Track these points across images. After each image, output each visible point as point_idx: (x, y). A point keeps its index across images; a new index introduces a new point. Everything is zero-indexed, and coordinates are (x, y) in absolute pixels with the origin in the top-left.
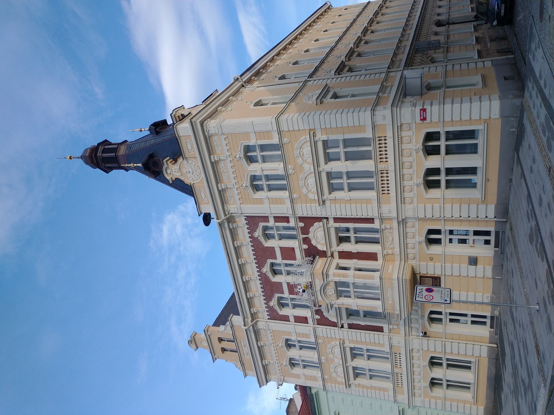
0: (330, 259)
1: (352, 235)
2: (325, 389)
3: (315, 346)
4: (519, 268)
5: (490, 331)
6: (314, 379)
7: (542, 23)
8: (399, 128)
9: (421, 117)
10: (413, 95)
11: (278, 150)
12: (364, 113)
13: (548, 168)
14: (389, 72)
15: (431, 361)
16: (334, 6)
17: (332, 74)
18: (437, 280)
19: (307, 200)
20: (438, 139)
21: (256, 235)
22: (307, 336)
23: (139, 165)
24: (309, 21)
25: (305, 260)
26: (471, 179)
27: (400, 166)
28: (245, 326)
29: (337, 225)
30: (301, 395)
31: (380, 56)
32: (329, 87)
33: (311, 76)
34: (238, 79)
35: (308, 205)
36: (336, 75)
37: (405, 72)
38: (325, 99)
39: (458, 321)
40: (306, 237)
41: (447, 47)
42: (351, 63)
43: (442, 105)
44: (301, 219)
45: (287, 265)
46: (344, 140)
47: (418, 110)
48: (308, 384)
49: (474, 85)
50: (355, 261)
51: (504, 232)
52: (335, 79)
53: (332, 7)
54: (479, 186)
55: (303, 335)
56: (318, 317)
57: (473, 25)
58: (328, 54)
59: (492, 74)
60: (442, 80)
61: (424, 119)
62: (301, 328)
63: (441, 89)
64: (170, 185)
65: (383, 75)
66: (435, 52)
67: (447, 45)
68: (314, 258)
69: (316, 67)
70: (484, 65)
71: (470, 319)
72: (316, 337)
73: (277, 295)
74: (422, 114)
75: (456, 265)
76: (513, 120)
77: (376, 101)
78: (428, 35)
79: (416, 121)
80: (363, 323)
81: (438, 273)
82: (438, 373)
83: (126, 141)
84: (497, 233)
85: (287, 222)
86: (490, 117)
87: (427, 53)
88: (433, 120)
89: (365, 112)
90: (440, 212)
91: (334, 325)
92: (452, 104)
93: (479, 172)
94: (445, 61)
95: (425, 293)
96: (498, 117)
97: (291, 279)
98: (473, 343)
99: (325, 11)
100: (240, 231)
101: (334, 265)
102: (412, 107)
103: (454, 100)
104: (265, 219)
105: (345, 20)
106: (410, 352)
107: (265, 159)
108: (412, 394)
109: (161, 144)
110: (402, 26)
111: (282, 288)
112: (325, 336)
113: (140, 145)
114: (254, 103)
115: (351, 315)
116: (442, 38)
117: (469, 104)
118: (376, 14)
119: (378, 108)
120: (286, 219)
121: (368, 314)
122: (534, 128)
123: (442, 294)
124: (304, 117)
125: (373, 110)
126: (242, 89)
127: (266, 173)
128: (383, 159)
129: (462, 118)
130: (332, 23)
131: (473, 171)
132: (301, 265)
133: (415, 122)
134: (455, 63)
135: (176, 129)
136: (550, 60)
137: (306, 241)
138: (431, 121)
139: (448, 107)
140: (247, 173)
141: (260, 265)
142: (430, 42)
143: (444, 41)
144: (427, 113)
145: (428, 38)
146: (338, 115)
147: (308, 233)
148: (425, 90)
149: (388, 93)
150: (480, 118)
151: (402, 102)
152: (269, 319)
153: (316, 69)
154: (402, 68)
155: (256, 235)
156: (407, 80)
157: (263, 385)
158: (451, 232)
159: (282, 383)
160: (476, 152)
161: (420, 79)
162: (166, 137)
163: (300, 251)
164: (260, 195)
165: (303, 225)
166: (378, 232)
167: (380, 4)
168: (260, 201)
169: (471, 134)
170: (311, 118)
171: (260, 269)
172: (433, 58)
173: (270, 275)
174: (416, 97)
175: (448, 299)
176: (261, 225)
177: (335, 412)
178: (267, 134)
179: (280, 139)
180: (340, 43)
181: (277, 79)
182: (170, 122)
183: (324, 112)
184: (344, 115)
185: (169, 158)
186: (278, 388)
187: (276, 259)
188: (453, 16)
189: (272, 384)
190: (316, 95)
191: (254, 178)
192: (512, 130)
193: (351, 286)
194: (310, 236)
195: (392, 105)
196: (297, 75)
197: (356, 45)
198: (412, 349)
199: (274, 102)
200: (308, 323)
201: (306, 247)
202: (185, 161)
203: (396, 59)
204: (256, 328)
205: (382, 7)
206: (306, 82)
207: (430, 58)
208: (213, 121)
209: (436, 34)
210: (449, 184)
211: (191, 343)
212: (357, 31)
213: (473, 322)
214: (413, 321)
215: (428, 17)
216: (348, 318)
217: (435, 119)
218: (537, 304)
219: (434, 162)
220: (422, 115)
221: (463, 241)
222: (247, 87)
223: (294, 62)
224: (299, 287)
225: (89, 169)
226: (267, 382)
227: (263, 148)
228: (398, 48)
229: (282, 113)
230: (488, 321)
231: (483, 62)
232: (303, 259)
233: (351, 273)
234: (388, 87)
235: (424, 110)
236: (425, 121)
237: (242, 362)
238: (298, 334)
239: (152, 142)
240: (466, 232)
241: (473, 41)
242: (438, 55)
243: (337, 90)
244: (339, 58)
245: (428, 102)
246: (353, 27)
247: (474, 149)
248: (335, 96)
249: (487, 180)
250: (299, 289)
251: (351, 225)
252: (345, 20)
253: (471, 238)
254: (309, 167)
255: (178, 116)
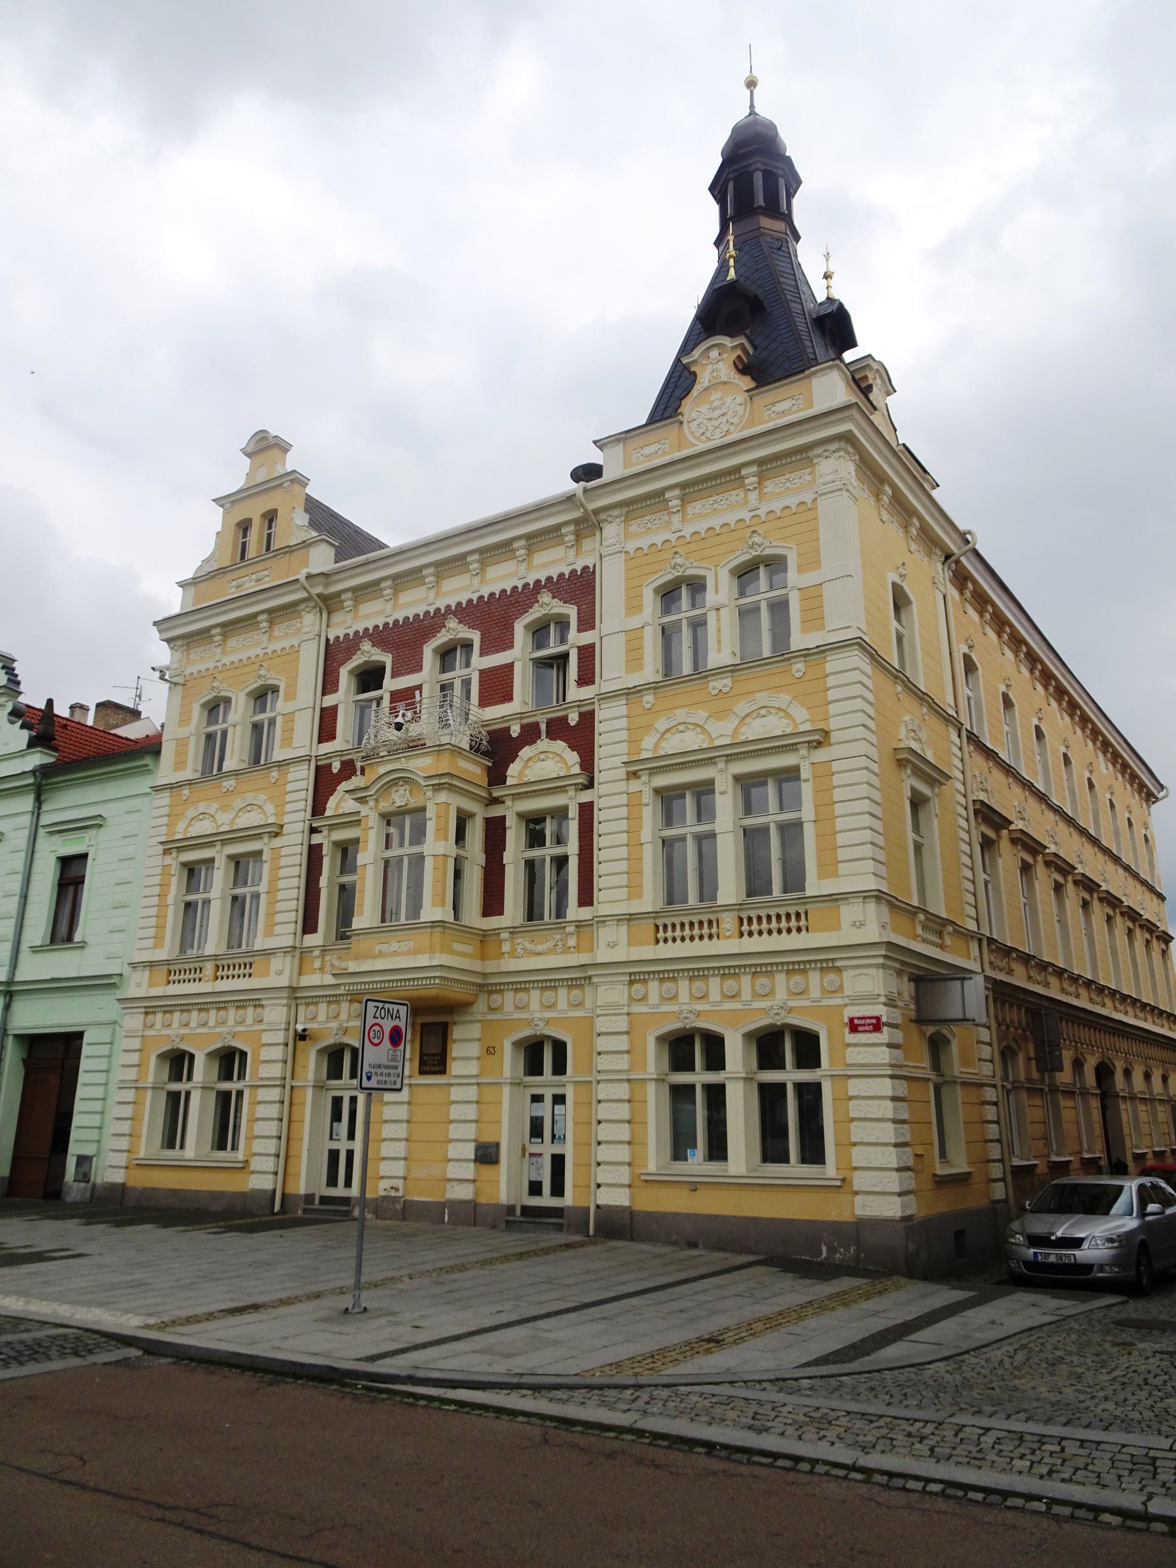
0: (484, 794)
1: (549, 851)
2: (157, 789)
3: (262, 762)
4: (463, 1265)
5: (314, 1194)
6: (180, 765)
7: (1112, 1325)
8: (830, 965)
9: (859, 1018)
10: (918, 999)
11: (774, 648)
12: (872, 871)
13: (720, 1338)
14: (980, 940)
15: (235, 1053)
16: (1154, 808)
17: (977, 793)
18: (439, 1065)
19: (635, 735)
20: (800, 1064)
21: (545, 597)
22: (287, 741)
23: (732, 274)
24: (1118, 743)
25: (481, 729)
26: (694, 1146)
27: (728, 968)
28: (309, 577)
29: (573, 812)
30: (147, 736)
31: (1021, 921)
32: (941, 784)
33: (973, 739)
34: (968, 542)
35: (624, 735)
36: (974, 805)
37: (980, 979)
38: (909, 771)
39: (336, 1116)
40: (540, 732)
41: (1041, 1090)
42: (1005, 844)
43: (890, 1072)
44: (588, 719)
45: (467, 683)
46: (798, 825)
47: (880, 1010)
48: (167, 749)
49: (943, 1154)
50: (481, 859)
51: (559, 1228)
52: (962, 800)
53: (1154, 803)
54: (679, 1166)
55: (289, 731)
56: (336, 767)
57: (1100, 1158)
58: (1029, 787)
59: (972, 1200)
60: (956, 1073)
61: (854, 1027)
62: (306, 726)
63: (934, 1071)
64: (678, 360)
65: (972, 926)
66: (1030, 1059)
67: (1047, 1090)
68: (485, 754)
69: (997, 754)
70: (996, 1180)
71: (343, 1146)
72: (283, 764)
73: (387, 659)
74: (868, 1021)
75: (471, 1112)
76: (849, 1252)
77: (902, 905)
78: (1076, 1042)
79: (849, 1008)
80: (323, 881)
81: (455, 1068)
82: (203, 1072)
83: (797, 238)
84: (558, 1212)
85: (579, 679)
86: (857, 1193)
87: (1027, 1040)
88: (850, 1049)
89: (874, 874)
90: (610, 1071)
91: (318, 808)
92: (894, 1099)
93: (714, 1167)
94: (1006, 1084)
95: (388, 1025)
96: (859, 1212)
97: (428, 698)
98: (282, 1154)
99: (1142, 786)
100: (557, 553)
101: (469, 805)
102: (886, 996)
103: (904, 1104)
104: (587, 622)
105: (1117, 833)
106: (252, 1001)
107: (747, 614)
108: (150, 1007)
109: (790, 334)
110: (1098, 978)
111: (408, 673)
112: (289, 787)
113: (787, 275)
114: (903, 584)
115: (345, 852)
116: (1065, 1077)
117: (893, 1141)
118: (1132, 915)
119: (885, 909)
120: (586, 678)
121: (346, 896)
122: (828, 1302)
123: (387, 1067)
124: (862, 714)
125: (879, 896)
126: (938, 552)
127: (711, 617)
128: (746, 925)
129: (855, 1123)
130: (1110, 800)
131: (718, 1149)
132: (467, 719)
133: (846, 1005)
134: (1001, 1108)
135: (831, 367)
136: (1010, 1344)
137: (530, 734)
138: (849, 1045)
139: (886, 1087)
140: (710, 566)
141: (467, 612)
142: (1058, 1045)
143: (1058, 1083)
144: (868, 1035)
145: (1067, 1042)
146: (865, 805)
147: (552, 735)
148: (930, 1030)
149: (924, 935)
150: (856, 1169)
151: (899, 973)
152: (328, 640)
153: (990, 754)
154: (990, 973)
155: (545, 597)
156: (959, 983)
157: (160, 631)
158: (559, 1099)
159: (166, 680)
160: (765, 1159)
161: (960, 1016)
162: (808, 344)
163: (503, 717)
164: (650, 601)
165: (573, 723)
166: (558, 917)
167: (1158, 924)
168: (633, 606)
169: (813, 1152)
170: (860, 732)
171: (455, 613)
172: (1014, 1054)
173: (442, 638)
174: (913, 1007)
175: (373, 1083)
176: (572, 612)
177: (100, 816)
178: (815, 619)
179: (806, 654)
180: (1058, 818)
181: (966, 650)
182: (849, 356)
183: (875, 767)
184: (867, 820)
185: (751, 351)
186: (153, 669)
187: (481, 655)
188: (1122, 1107)
189: (162, 654)
190: (923, 750)
191: (697, 586)
192: (824, 1249)
193: (415, 849)
194: (544, 744)
195: (890, 945)
196: (976, 704)
197: (1053, 859)
198: (262, 1006)
199: (905, 641)
200: (320, 742)
201: (515, 731)
202: (741, 397)
203: (1013, 959)
204: (302, 607)
205: (1151, 932)
206: (955, 726)
207: (1013, 1045)
208: (852, 467)
209: (1078, 1065)
210: (681, 1094)
211: (259, 441)
212: (1091, 864)
213: (334, 1155)
214: (333, 1006)
215: (1124, 1044)
216: (336, 844)
217: (854, 1056)
218: (365, 1309)
219: (737, 1055)
220: (863, 1022)
221: (536, 1128)
222: (946, 569)
223: (1011, 696)
224: (409, 714)
225: (721, 137)
226: (168, 641)
227: (780, 608)
228: (1044, 966)
229: (874, 657)
230: (340, 1191)
231: (1003, 1180)
232: (483, 726)
233: (448, 846)
234: (941, 937)
235: (877, 1026)
236: (847, 1030)
237: (215, 576)
238: (289, 717)
239: (793, 305)
240: (559, 1138)
241: (1058, 1155)
242: (1022, 1068)
243: (935, 806)
244: (1019, 815)
245: (898, 1036)
246: (1100, 856)
247: (772, 1149)
248: (918, 803)
249: (694, 1187)
250: (404, 715)
251: (572, 848)
252: (1117, 833)
253: (547, 1149)
254: (722, 732)
255: (866, 377)
